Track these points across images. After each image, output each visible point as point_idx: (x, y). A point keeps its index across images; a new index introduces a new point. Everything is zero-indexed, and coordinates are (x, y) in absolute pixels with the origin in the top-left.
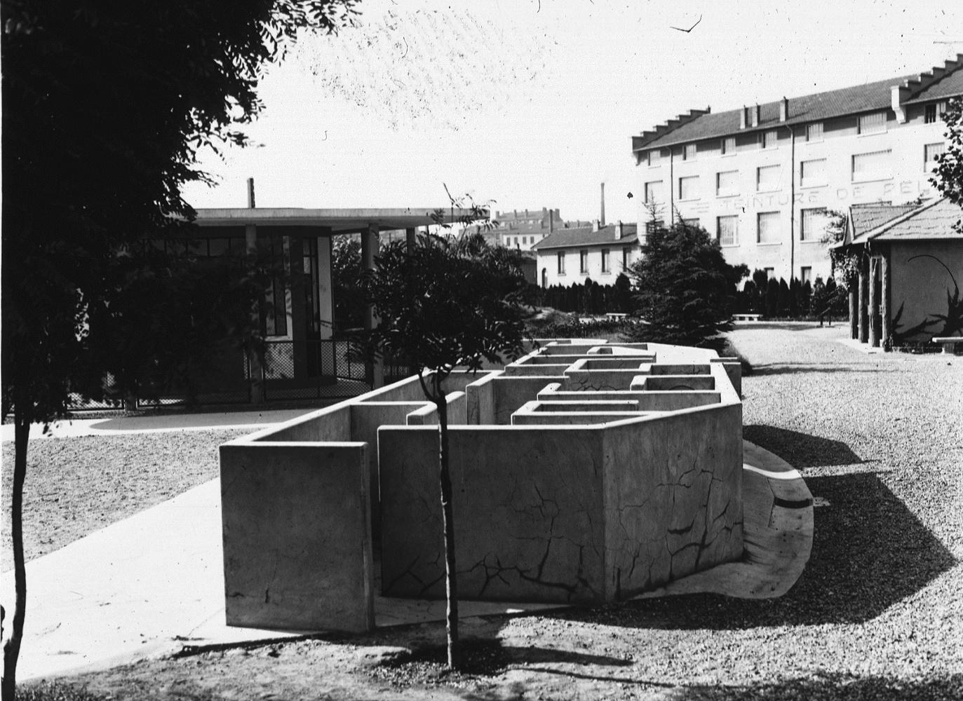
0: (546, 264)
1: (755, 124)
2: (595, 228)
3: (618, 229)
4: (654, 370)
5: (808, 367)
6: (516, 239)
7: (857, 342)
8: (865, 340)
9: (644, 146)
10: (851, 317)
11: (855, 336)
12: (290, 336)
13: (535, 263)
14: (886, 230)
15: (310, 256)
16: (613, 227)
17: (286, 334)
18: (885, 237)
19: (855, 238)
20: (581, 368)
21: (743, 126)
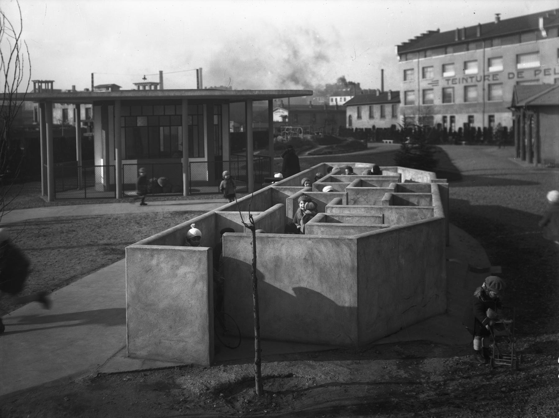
0: (351, 112)
1: (463, 39)
2: (378, 94)
3: (389, 94)
4: (399, 188)
5: (521, 31)
6: (336, 99)
7: (520, 159)
8: (524, 159)
9: (406, 50)
10: (516, 141)
11: (518, 155)
12: (206, 159)
13: (345, 112)
14: (536, 99)
15: (218, 115)
16: (387, 93)
17: (204, 157)
18: (532, 103)
19: (518, 103)
20: (355, 186)
21: (457, 40)
